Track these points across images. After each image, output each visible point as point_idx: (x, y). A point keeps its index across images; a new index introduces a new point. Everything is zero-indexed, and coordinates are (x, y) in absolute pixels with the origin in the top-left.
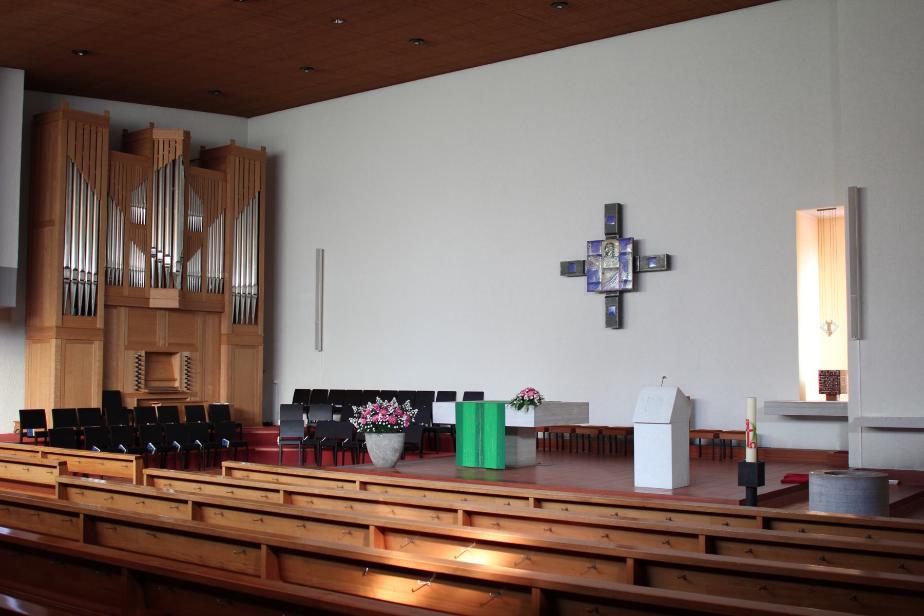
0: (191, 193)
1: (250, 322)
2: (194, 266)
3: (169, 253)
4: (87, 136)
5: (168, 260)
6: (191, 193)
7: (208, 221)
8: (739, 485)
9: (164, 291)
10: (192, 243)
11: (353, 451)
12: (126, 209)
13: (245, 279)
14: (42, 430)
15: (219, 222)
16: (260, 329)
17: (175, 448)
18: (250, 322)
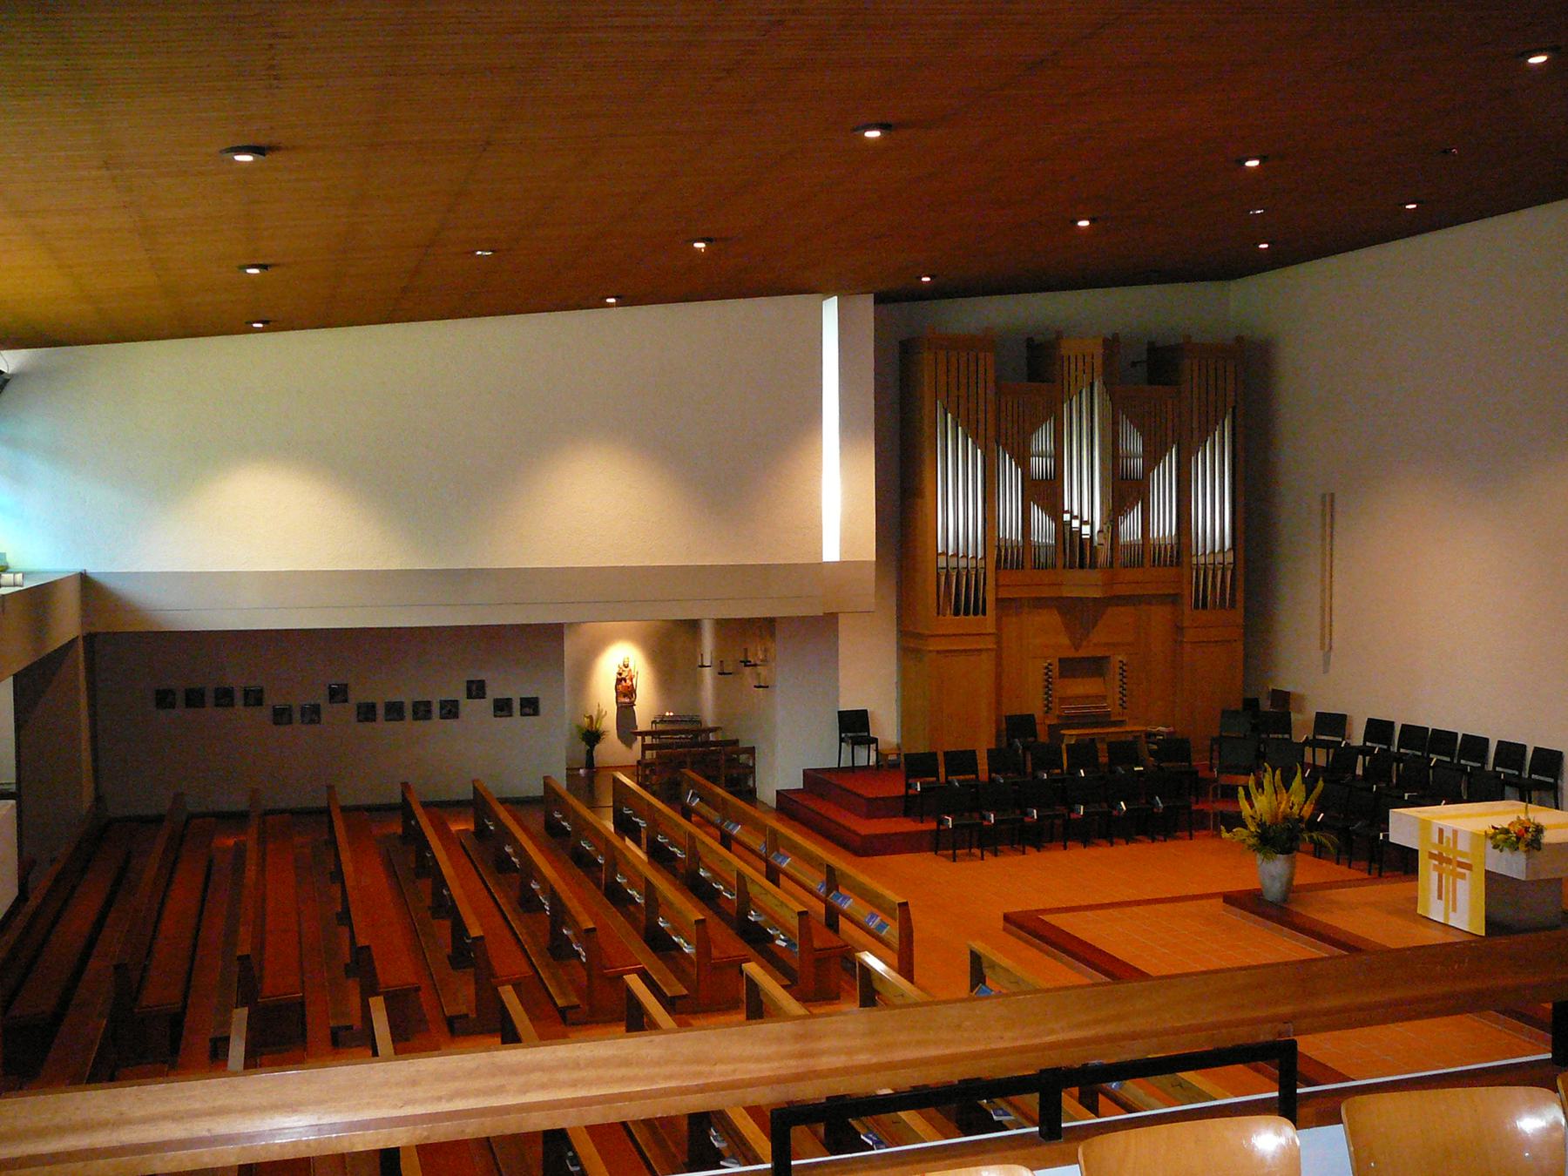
0: (1123, 418)
1: (1222, 605)
2: (1131, 527)
3: (1084, 502)
4: (972, 365)
5: (1086, 530)
6: (1123, 418)
7: (1153, 457)
8: (808, 774)
9: (1081, 574)
10: (1125, 492)
11: (247, 693)
12: (1023, 461)
13: (1214, 518)
14: (1551, 780)
15: (1171, 460)
16: (1238, 615)
17: (1155, 805)
18: (1222, 605)
